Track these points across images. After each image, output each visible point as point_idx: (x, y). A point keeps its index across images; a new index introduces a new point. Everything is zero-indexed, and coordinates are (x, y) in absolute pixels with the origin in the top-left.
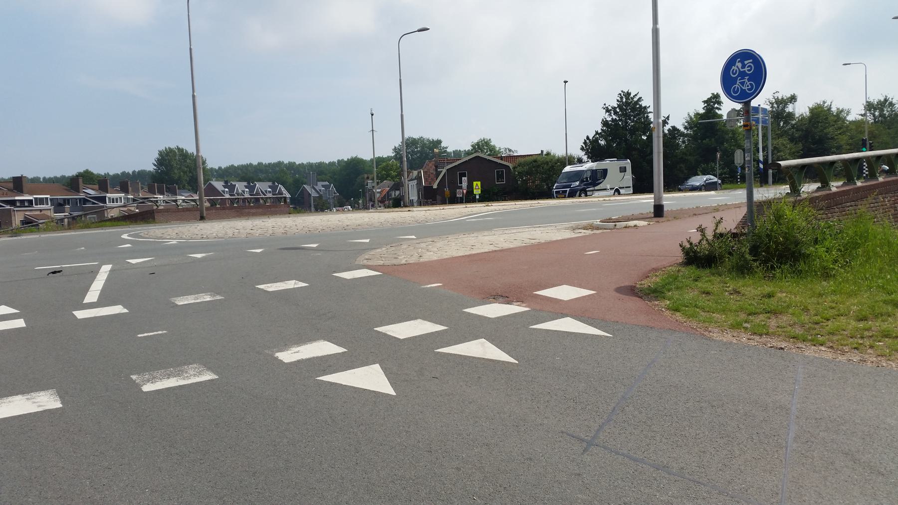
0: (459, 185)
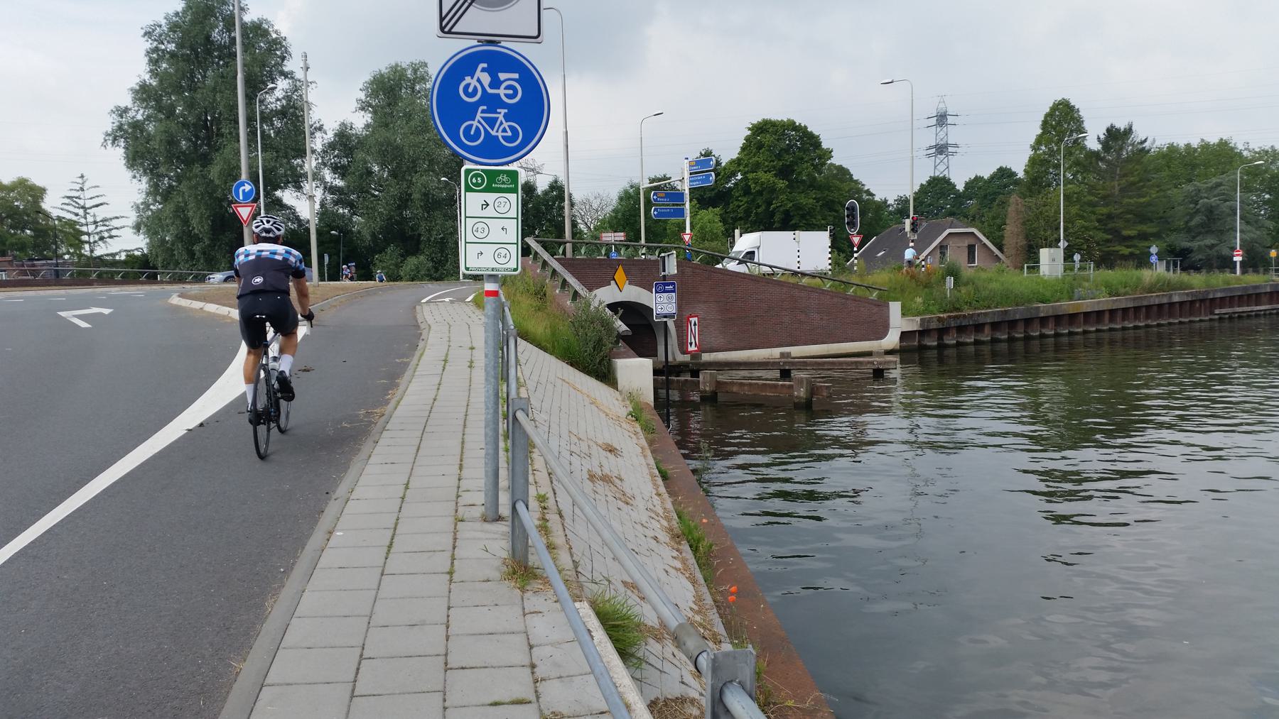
0: (1026, 265)
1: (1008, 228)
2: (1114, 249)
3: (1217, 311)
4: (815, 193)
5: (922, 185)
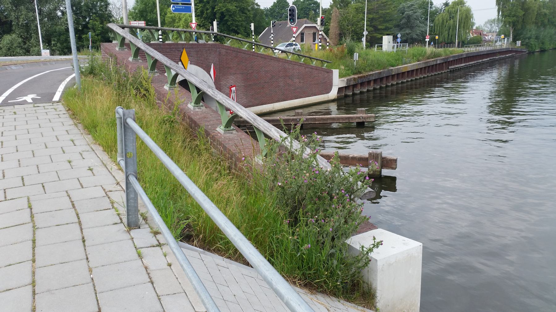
1: (332, 24)
2: (374, 35)
3: (450, 68)
4: (236, 4)
5: (274, 3)
